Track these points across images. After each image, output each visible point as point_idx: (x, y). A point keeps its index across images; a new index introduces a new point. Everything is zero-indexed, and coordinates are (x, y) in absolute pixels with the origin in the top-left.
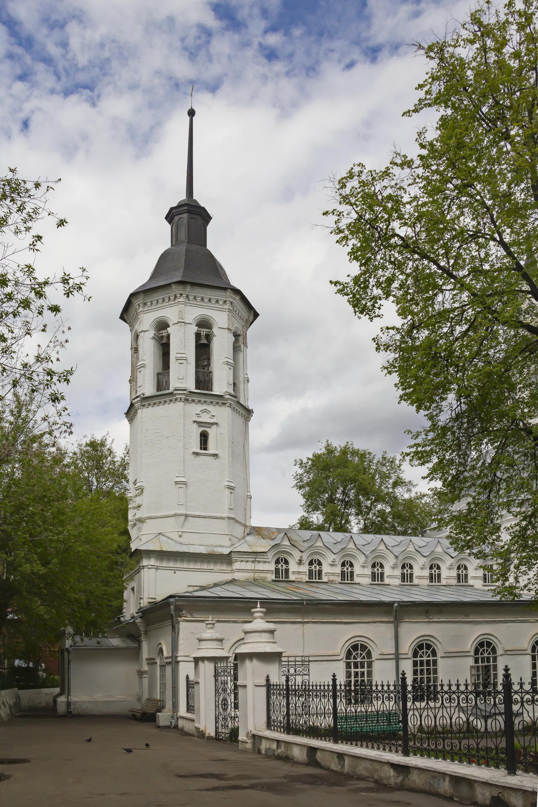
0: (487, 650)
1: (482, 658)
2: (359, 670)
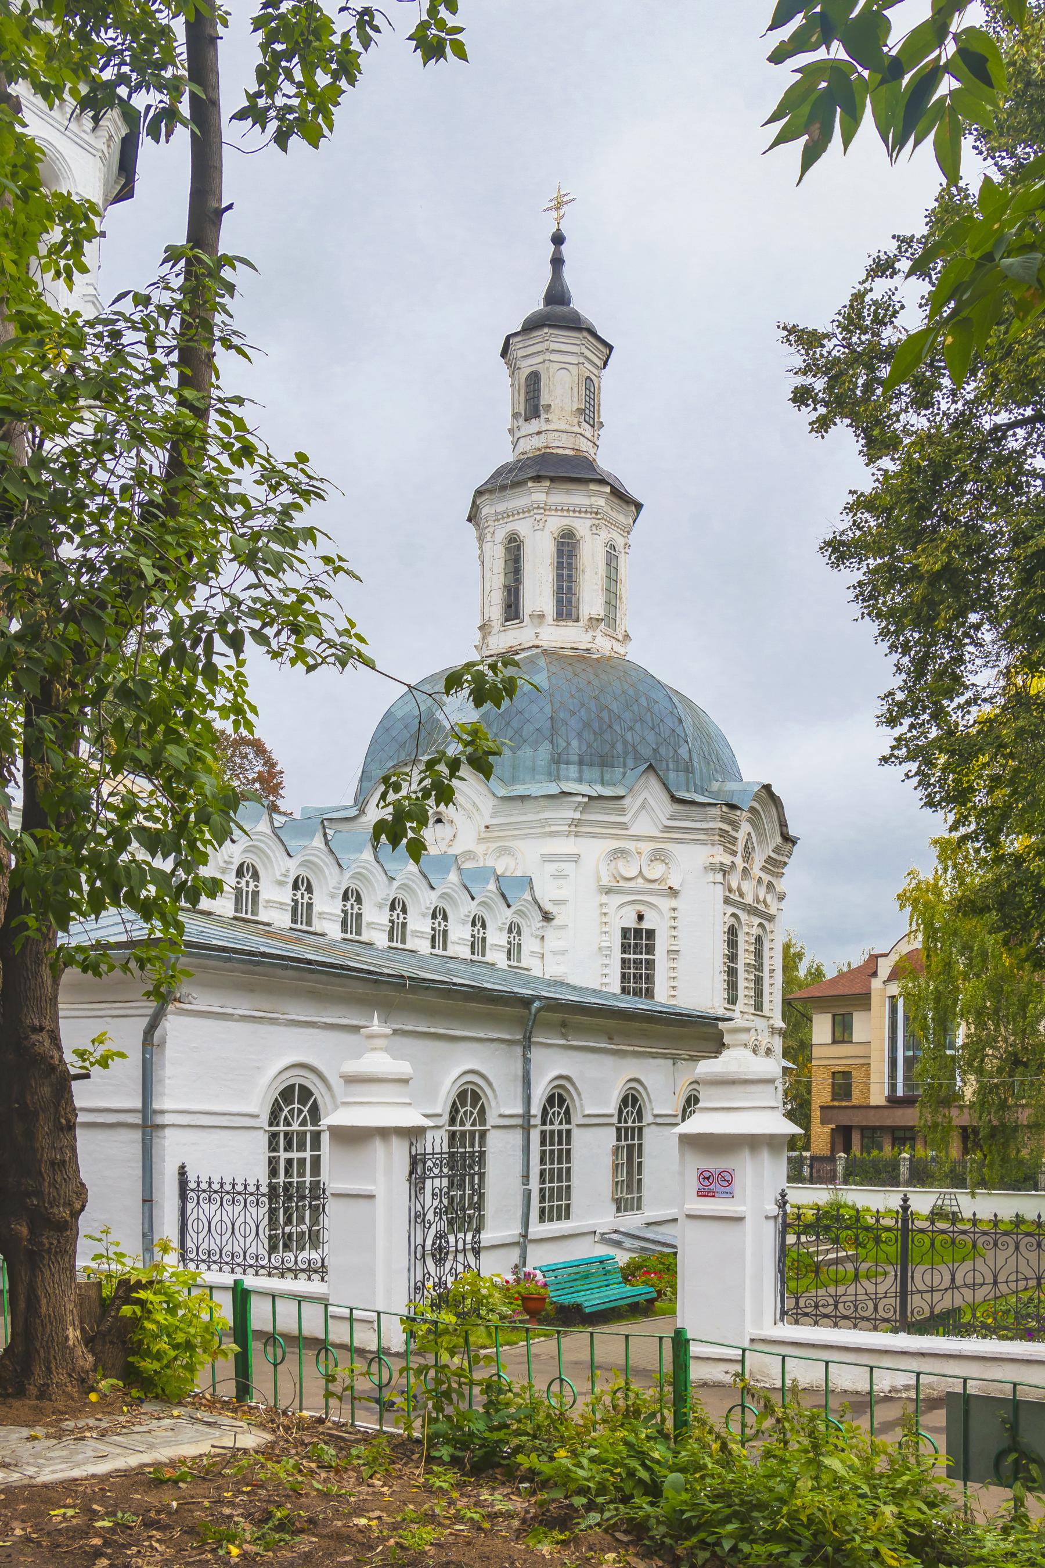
0: (300, 1111)
1: (286, 1134)
2: (295, 1155)
